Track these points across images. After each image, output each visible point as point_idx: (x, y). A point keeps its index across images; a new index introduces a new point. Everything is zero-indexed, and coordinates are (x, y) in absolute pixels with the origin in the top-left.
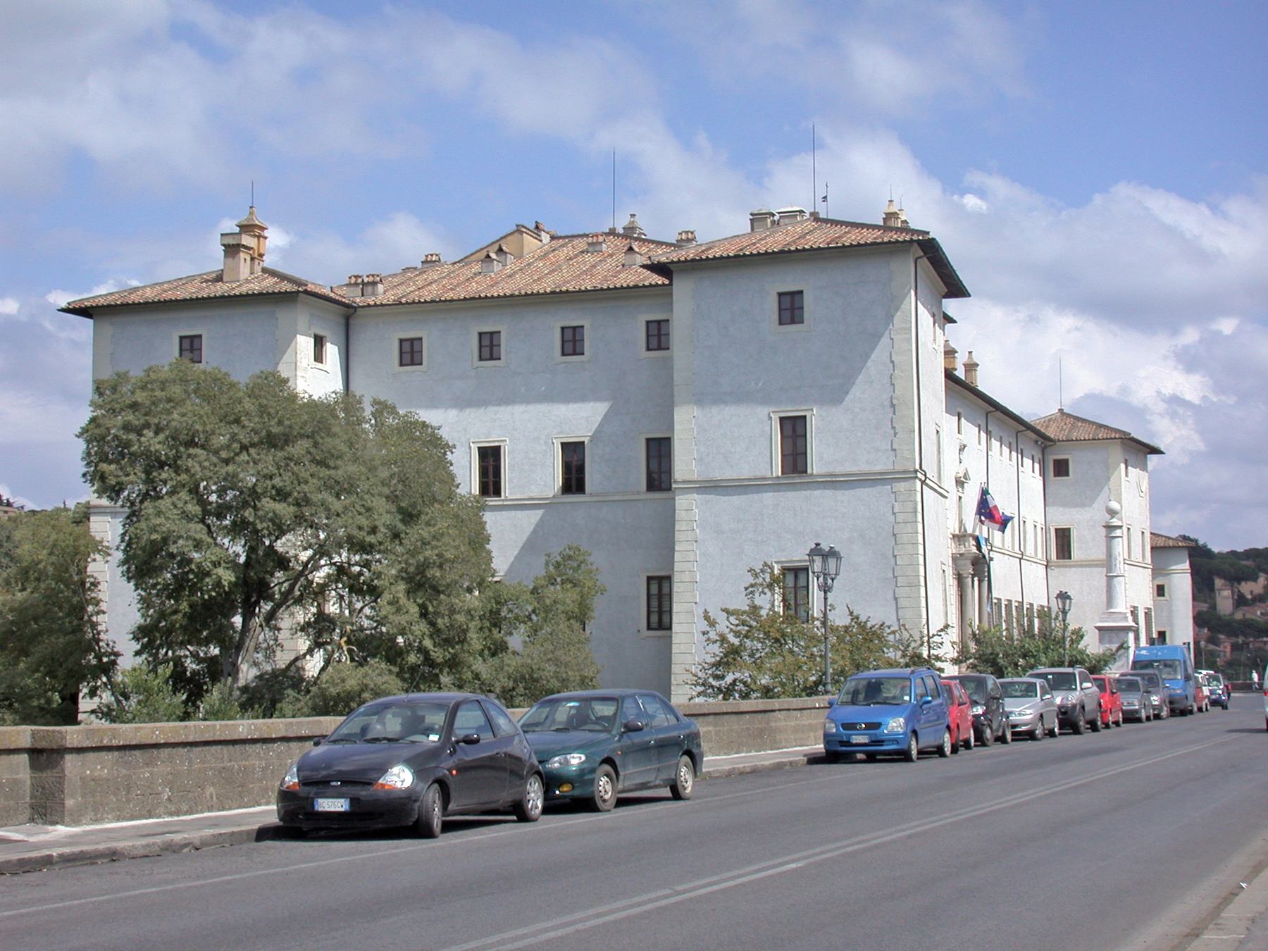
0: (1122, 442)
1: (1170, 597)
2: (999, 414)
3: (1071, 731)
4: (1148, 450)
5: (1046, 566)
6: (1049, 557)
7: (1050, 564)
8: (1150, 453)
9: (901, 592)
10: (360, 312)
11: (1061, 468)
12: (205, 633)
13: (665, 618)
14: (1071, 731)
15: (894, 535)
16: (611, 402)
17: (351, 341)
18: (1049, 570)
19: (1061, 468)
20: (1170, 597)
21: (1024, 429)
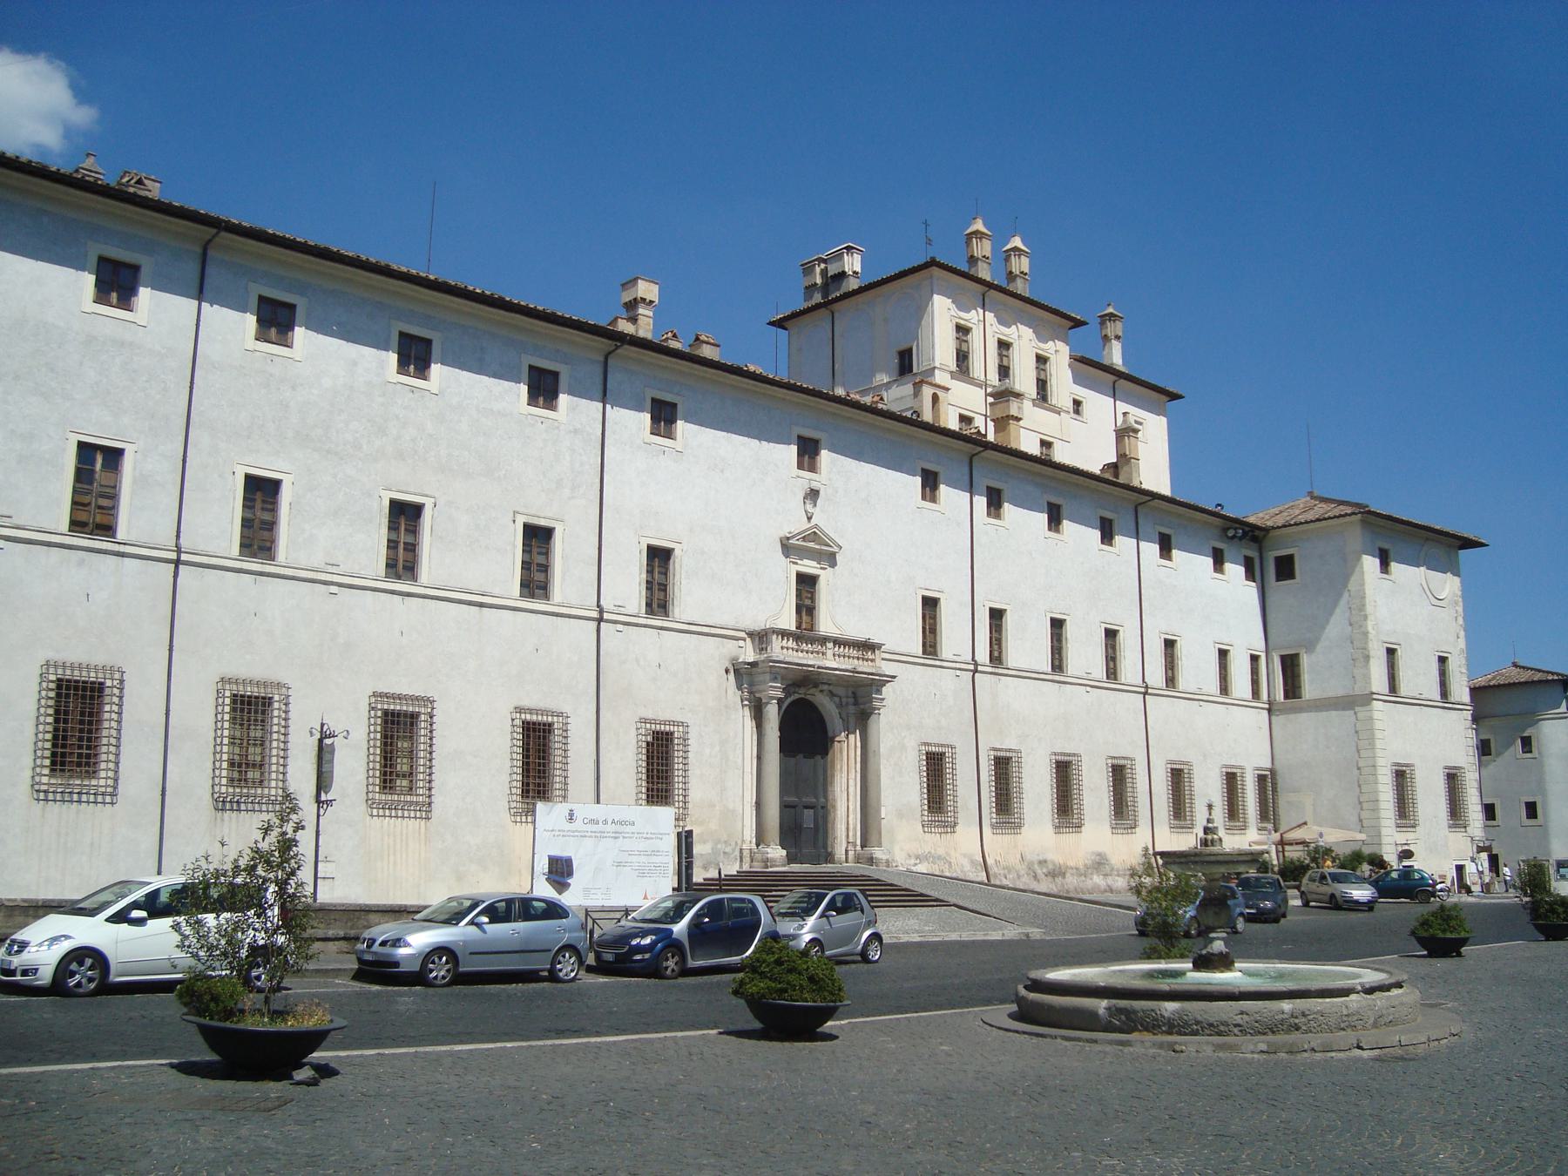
0: (1363, 521)
1: (1539, 753)
2: (990, 454)
3: (1425, 953)
4: (1459, 543)
5: (1269, 711)
6: (1272, 695)
7: (1275, 707)
8: (1462, 547)
9: (1365, 815)
10: (1273, 533)
11: (1285, 568)
12: (744, 1104)
13: (60, 715)
14: (1425, 953)
15: (1357, 732)
16: (99, 452)
17: (1267, 595)
18: (1273, 718)
19: (1285, 568)
20: (1539, 753)
21: (982, 449)
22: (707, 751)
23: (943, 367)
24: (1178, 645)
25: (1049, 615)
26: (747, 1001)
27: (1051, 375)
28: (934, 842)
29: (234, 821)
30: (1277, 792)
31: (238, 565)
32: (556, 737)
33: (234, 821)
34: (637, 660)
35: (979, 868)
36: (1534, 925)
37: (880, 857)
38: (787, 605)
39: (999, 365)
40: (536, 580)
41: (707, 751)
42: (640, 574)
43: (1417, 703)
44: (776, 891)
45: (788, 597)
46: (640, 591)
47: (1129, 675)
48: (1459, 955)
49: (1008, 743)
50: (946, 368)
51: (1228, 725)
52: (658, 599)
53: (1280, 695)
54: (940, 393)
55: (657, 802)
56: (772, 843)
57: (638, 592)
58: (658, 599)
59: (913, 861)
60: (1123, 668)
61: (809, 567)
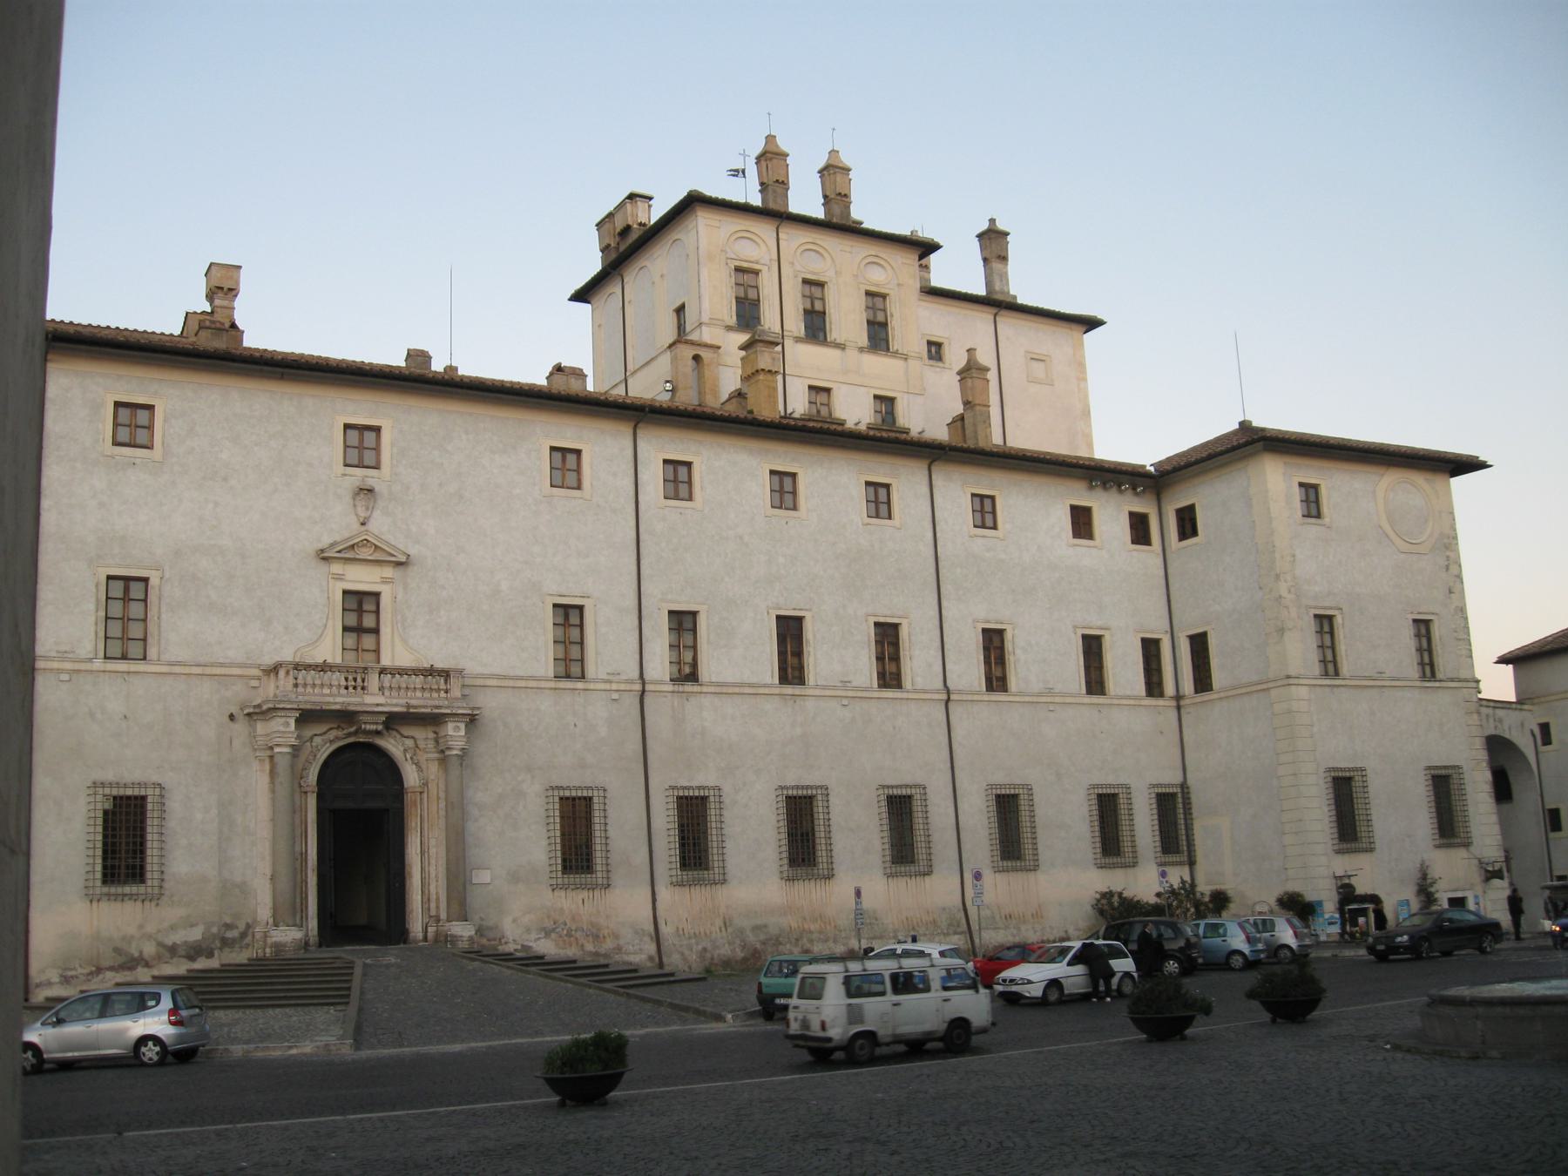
22: (199, 816)
23: (715, 322)
24: (1008, 636)
25: (1080, 632)
26: (1263, 1003)
27: (892, 316)
28: (573, 903)
29: (818, 886)
30: (1191, 814)
31: (876, 695)
32: (917, 806)
33: (818, 886)
34: (92, 715)
35: (647, 939)
36: (1132, 1019)
37: (460, 934)
38: (329, 632)
39: (806, 311)
40: (890, 675)
41: (199, 816)
42: (97, 611)
43: (1376, 683)
44: (298, 976)
45: (330, 623)
46: (96, 633)
47: (919, 680)
48: (1184, 1038)
49: (700, 778)
50: (719, 323)
51: (232, 717)
52: (996, 680)
53: (1188, 685)
54: (704, 353)
55: (577, 868)
56: (281, 924)
57: (93, 634)
58: (996, 680)
59: (533, 936)
60: (908, 671)
61: (362, 578)
